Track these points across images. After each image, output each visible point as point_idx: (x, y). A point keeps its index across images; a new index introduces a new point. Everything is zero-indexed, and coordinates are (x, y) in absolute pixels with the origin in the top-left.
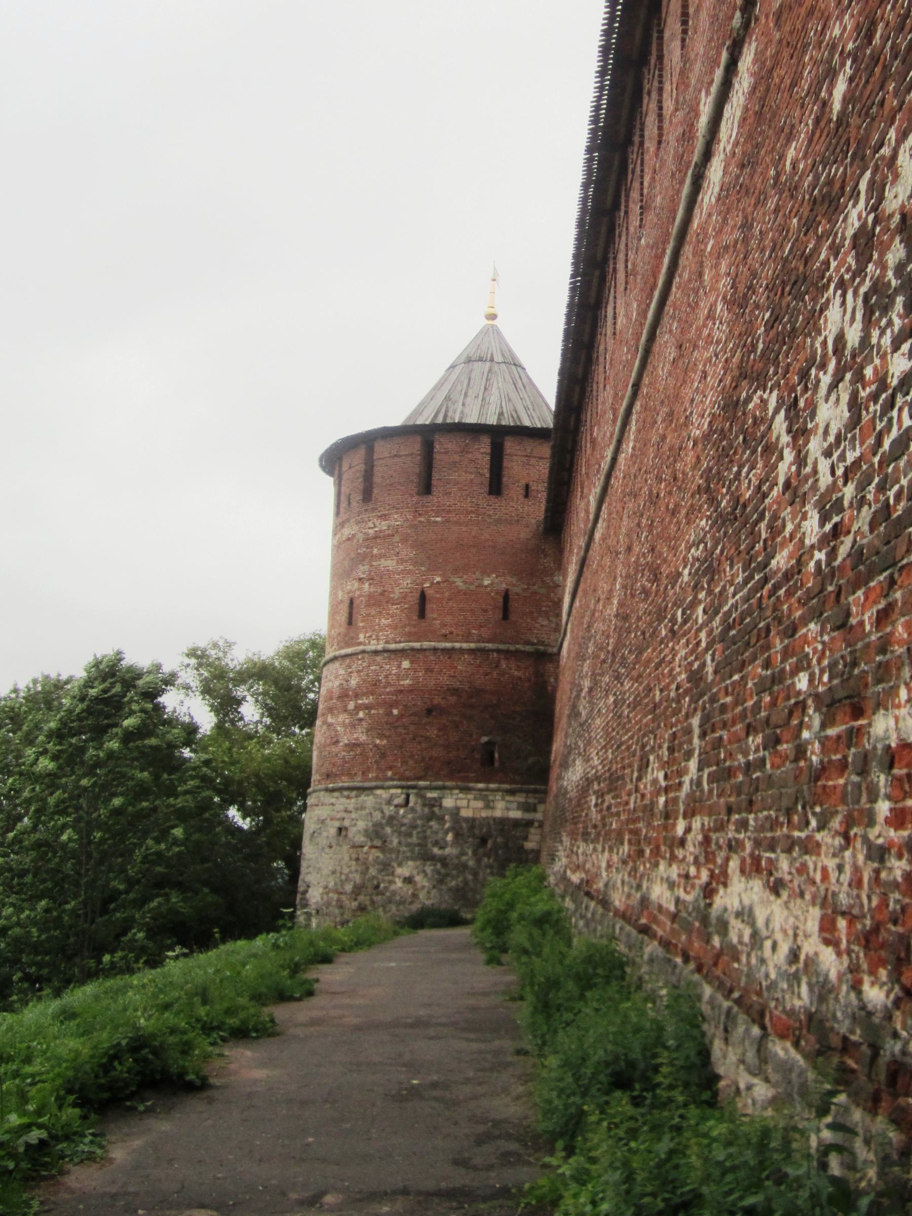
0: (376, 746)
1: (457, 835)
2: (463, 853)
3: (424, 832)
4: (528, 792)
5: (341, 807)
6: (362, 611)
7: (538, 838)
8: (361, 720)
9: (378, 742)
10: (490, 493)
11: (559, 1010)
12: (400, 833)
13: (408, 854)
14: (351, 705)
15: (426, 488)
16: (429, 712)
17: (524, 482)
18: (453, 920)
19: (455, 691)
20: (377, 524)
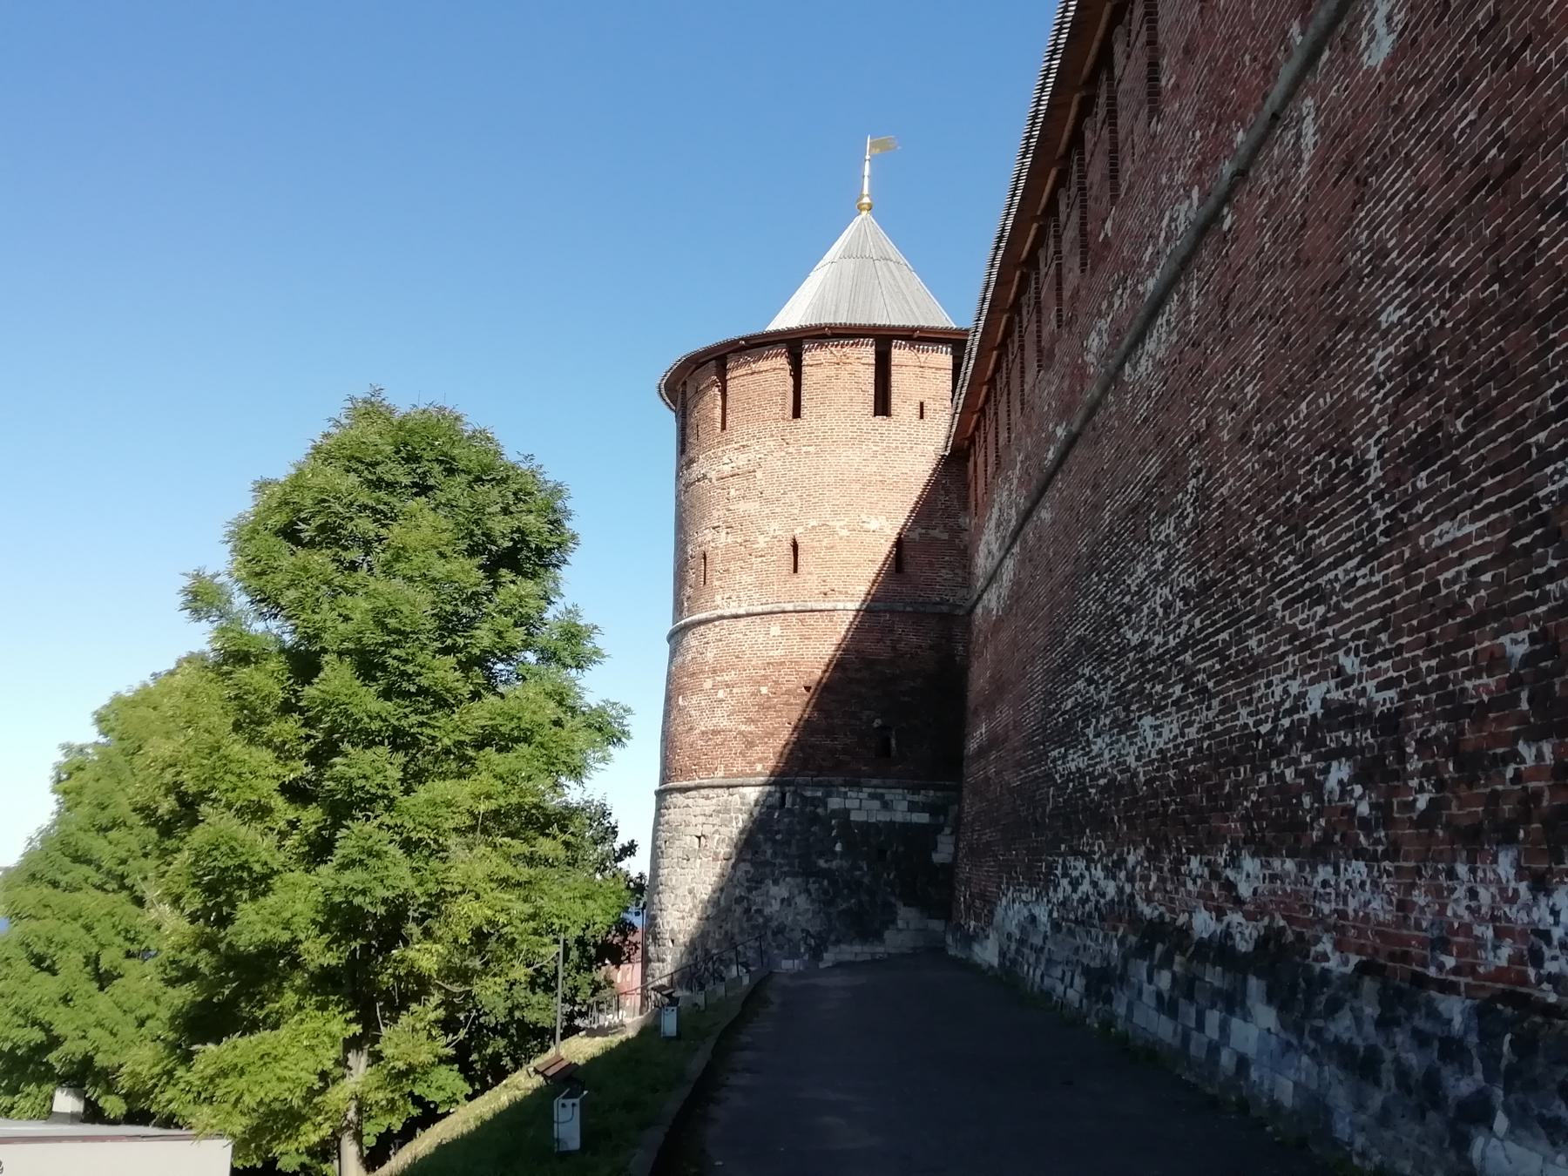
0: (740, 733)
2: (854, 867)
7: (952, 849)
8: (721, 701)
13: (786, 869)
14: (708, 684)
15: (797, 413)
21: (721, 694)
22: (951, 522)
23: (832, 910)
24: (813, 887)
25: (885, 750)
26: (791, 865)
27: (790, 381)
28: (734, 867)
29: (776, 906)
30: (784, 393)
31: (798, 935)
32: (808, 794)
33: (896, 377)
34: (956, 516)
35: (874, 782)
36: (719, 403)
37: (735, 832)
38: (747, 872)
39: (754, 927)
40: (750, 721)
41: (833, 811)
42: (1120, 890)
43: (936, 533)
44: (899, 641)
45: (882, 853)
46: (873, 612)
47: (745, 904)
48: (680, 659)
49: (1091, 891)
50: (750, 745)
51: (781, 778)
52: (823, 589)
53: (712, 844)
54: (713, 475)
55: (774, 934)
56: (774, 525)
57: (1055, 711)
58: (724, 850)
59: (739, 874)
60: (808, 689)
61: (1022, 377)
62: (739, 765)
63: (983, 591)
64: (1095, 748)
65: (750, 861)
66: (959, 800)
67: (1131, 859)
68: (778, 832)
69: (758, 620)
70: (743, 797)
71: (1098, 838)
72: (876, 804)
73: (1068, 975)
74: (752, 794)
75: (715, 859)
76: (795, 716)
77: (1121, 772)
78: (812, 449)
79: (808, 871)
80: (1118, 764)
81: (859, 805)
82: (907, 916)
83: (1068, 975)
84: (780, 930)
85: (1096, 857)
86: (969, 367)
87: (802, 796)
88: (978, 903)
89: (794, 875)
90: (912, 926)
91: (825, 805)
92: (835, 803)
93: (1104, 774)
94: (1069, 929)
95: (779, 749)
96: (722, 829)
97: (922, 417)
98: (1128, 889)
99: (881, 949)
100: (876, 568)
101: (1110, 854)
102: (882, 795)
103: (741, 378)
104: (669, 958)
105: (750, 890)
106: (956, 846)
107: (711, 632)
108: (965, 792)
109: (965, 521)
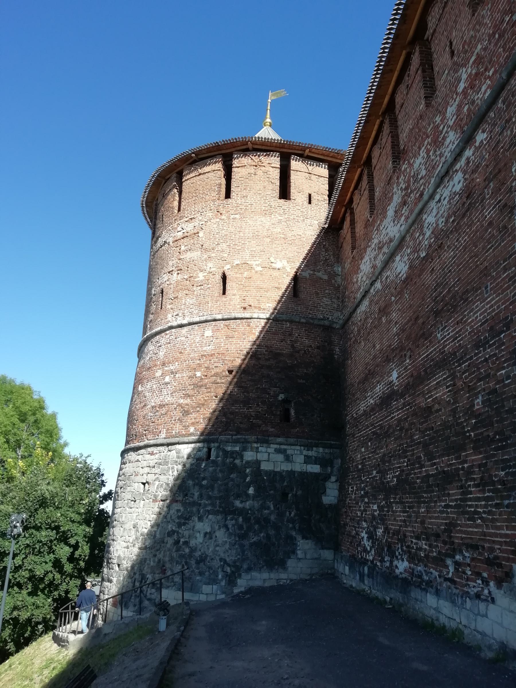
0: (180, 405)
2: (263, 507)
3: (226, 484)
4: (325, 446)
7: (336, 493)
8: (167, 384)
10: (280, 198)
12: (201, 486)
13: (209, 508)
14: (159, 374)
15: (228, 195)
17: (307, 192)
18: (105, 634)
20: (184, 227)
21: (167, 379)
22: (329, 269)
23: (246, 543)
24: (230, 523)
25: (286, 417)
26: (213, 505)
27: (224, 181)
28: (169, 507)
29: (200, 538)
30: (220, 184)
31: (216, 563)
32: (229, 449)
33: (294, 177)
34: (332, 266)
35: (279, 440)
36: (177, 198)
37: (171, 478)
38: (178, 511)
39: (182, 556)
40: (187, 396)
41: (248, 462)
43: (320, 274)
44: (296, 342)
45: (285, 495)
46: (277, 321)
47: (175, 537)
48: (142, 362)
50: (186, 413)
51: (207, 438)
52: (243, 305)
53: (153, 489)
54: (171, 240)
55: (198, 562)
56: (210, 265)
58: (162, 493)
59: (172, 512)
60: (230, 372)
62: (178, 428)
65: (181, 502)
68: (204, 479)
69: (196, 327)
72: (280, 457)
74: (186, 450)
75: (155, 501)
76: (221, 391)
78: (237, 216)
79: (227, 510)
81: (267, 457)
82: (304, 546)
84: (202, 560)
86: (340, 182)
89: (216, 513)
90: (308, 556)
91: (242, 457)
92: (249, 456)
95: (208, 415)
96: (162, 477)
97: (310, 202)
99: (283, 576)
100: (280, 293)
102: (285, 450)
103: (192, 181)
104: (115, 580)
105: (180, 525)
107: (162, 339)
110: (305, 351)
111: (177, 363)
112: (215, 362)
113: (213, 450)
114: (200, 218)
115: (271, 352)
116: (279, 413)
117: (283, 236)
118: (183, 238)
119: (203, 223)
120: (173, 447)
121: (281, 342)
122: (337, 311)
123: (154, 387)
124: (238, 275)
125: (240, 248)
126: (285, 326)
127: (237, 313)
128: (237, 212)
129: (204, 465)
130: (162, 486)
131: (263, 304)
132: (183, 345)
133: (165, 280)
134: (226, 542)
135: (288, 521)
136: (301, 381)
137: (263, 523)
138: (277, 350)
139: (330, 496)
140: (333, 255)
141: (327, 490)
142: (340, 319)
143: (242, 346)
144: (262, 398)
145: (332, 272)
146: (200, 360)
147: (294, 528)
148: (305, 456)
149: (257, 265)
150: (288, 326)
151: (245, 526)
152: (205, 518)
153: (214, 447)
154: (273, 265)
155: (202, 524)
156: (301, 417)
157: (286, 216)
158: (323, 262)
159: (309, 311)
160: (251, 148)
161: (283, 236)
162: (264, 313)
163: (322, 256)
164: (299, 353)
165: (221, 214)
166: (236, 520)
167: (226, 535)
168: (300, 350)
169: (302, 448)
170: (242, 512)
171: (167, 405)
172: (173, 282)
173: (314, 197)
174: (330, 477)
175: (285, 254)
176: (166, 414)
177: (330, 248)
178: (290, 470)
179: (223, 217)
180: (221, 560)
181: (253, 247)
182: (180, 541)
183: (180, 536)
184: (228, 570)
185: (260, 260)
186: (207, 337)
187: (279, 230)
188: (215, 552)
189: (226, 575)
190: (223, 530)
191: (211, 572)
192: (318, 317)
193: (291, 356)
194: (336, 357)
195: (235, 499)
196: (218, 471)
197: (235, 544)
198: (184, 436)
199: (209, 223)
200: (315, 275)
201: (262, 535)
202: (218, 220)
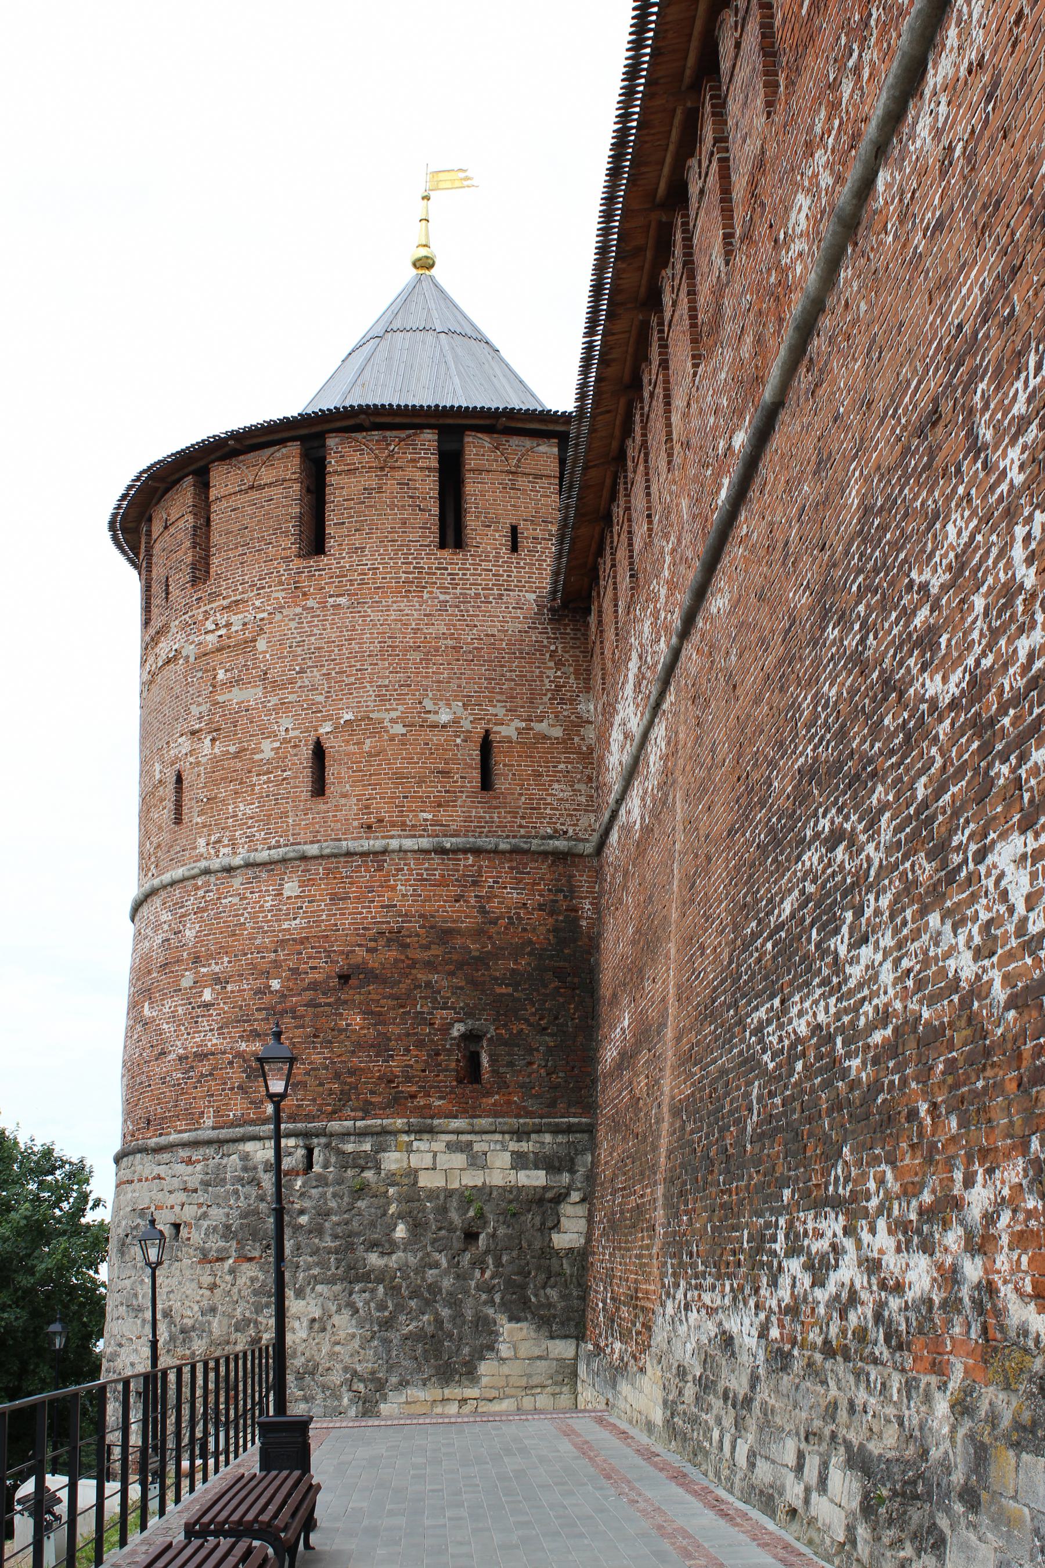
0: (239, 1055)
1: (417, 1227)
4: (556, 1130)
5: (176, 1183)
6: (195, 792)
7: (582, 1225)
8: (207, 1005)
9: (243, 1046)
10: (442, 546)
11: (228, 1227)
13: (315, 1271)
14: (187, 982)
15: (315, 542)
16: (344, 978)
19: (395, 938)
22: (566, 710)
23: (395, 1337)
25: (471, 1072)
26: (323, 1265)
32: (349, 1148)
33: (472, 488)
34: (572, 701)
38: (253, 1280)
42: (950, 1276)
43: (542, 727)
44: (489, 898)
49: (861, 1281)
56: (287, 722)
57: (755, 936)
61: (668, 404)
63: (620, 801)
64: (856, 972)
66: (593, 1146)
67: (979, 1198)
68: (302, 1212)
70: (245, 1157)
71: (876, 1160)
72: (459, 1160)
73: (812, 1465)
77: (932, 1000)
78: (343, 600)
79: (356, 1275)
80: (920, 984)
83: (812, 1465)
85: (874, 1203)
87: (340, 1153)
88: (625, 1312)
89: (331, 1281)
92: (392, 1161)
93: (884, 1017)
94: (810, 1364)
96: (214, 1211)
97: (514, 548)
98: (973, 1270)
101: (911, 1191)
102: (470, 1144)
106: (590, 1219)
108: (602, 1131)
109: (588, 707)
110: (510, 918)
111: (226, 959)
112: (309, 958)
113: (316, 1152)
114: (258, 603)
115: (432, 927)
116: (453, 1065)
117: (450, 642)
118: (219, 650)
119: (265, 615)
120: (232, 1147)
121: (457, 901)
122: (586, 811)
123: (180, 1012)
124: (352, 748)
125: (352, 679)
126: (462, 863)
127: (353, 839)
128: (341, 591)
129: (299, 1183)
130: (215, 1228)
131: (411, 815)
132: (237, 915)
133: (184, 752)
134: (353, 1336)
135: (478, 1288)
136: (503, 990)
137: (426, 1295)
138: (446, 922)
139: (569, 1235)
140: (577, 673)
141: (562, 1219)
142: (594, 830)
143: (366, 918)
144: (416, 1034)
145: (573, 717)
146: (276, 951)
147: (491, 1302)
148: (513, 1153)
149: (393, 721)
150: (470, 862)
151: (390, 1304)
152: (308, 1290)
153: (319, 1145)
154: (432, 717)
155: (303, 1303)
156: (502, 1070)
157: (458, 591)
158: (549, 695)
159: (518, 820)
160: (367, 424)
161: (450, 642)
162: (414, 836)
163: (546, 681)
164: (495, 924)
165: (305, 594)
166: (373, 1291)
167: (354, 1322)
168: (498, 918)
169: (507, 1137)
170: (382, 1276)
171: (213, 1054)
172: (204, 760)
173: (527, 531)
174: (568, 1194)
175: (459, 686)
176: (211, 1074)
177: (567, 655)
178: (480, 1184)
179: (310, 603)
180: (346, 1369)
181: (382, 677)
182: (261, 1338)
183: (262, 1328)
184: (361, 1387)
185: (401, 708)
186: (289, 898)
187: (443, 629)
188: (332, 1355)
189: (358, 1398)
190: (347, 1313)
191: (328, 1393)
192: (542, 832)
193: (478, 933)
194: (584, 923)
195: (367, 1251)
196: (329, 1195)
197: (372, 1337)
198: (252, 1123)
199: (278, 617)
200: (532, 729)
201: (426, 1318)
202: (299, 610)
